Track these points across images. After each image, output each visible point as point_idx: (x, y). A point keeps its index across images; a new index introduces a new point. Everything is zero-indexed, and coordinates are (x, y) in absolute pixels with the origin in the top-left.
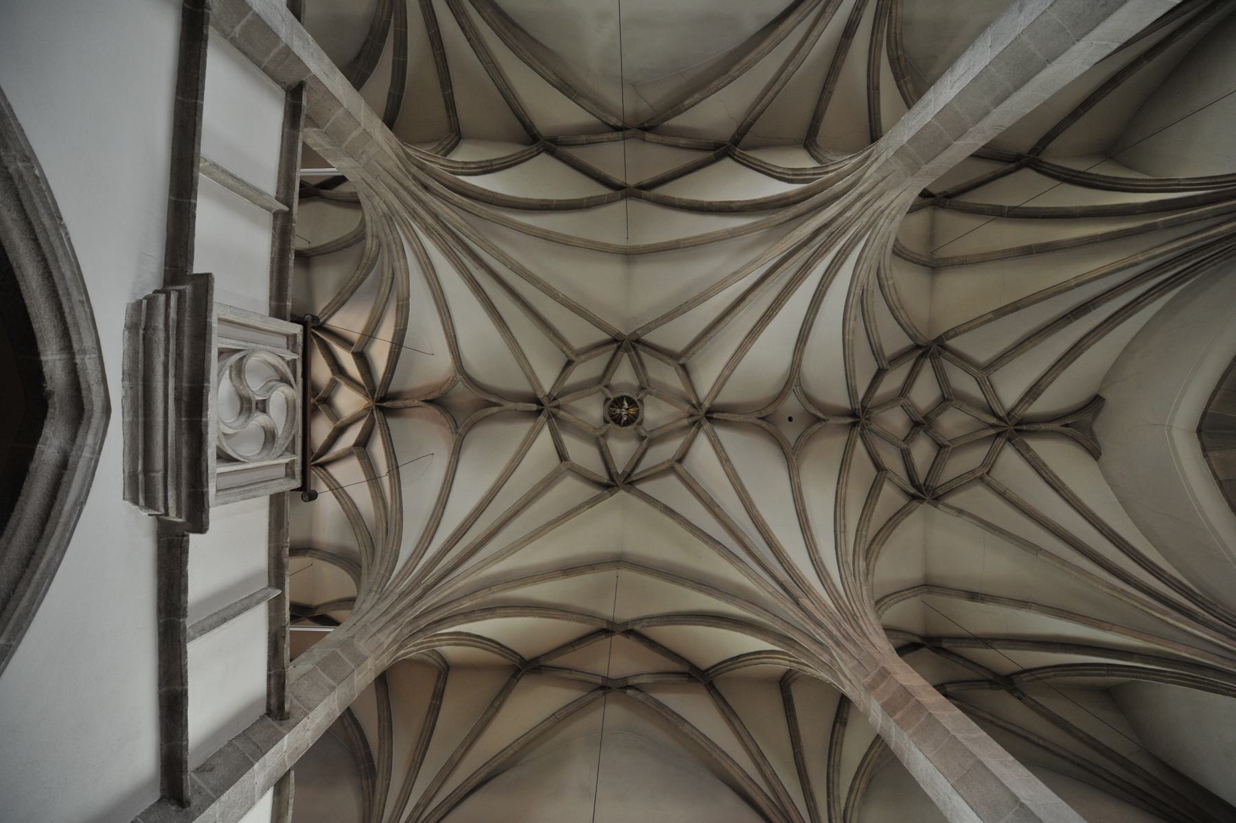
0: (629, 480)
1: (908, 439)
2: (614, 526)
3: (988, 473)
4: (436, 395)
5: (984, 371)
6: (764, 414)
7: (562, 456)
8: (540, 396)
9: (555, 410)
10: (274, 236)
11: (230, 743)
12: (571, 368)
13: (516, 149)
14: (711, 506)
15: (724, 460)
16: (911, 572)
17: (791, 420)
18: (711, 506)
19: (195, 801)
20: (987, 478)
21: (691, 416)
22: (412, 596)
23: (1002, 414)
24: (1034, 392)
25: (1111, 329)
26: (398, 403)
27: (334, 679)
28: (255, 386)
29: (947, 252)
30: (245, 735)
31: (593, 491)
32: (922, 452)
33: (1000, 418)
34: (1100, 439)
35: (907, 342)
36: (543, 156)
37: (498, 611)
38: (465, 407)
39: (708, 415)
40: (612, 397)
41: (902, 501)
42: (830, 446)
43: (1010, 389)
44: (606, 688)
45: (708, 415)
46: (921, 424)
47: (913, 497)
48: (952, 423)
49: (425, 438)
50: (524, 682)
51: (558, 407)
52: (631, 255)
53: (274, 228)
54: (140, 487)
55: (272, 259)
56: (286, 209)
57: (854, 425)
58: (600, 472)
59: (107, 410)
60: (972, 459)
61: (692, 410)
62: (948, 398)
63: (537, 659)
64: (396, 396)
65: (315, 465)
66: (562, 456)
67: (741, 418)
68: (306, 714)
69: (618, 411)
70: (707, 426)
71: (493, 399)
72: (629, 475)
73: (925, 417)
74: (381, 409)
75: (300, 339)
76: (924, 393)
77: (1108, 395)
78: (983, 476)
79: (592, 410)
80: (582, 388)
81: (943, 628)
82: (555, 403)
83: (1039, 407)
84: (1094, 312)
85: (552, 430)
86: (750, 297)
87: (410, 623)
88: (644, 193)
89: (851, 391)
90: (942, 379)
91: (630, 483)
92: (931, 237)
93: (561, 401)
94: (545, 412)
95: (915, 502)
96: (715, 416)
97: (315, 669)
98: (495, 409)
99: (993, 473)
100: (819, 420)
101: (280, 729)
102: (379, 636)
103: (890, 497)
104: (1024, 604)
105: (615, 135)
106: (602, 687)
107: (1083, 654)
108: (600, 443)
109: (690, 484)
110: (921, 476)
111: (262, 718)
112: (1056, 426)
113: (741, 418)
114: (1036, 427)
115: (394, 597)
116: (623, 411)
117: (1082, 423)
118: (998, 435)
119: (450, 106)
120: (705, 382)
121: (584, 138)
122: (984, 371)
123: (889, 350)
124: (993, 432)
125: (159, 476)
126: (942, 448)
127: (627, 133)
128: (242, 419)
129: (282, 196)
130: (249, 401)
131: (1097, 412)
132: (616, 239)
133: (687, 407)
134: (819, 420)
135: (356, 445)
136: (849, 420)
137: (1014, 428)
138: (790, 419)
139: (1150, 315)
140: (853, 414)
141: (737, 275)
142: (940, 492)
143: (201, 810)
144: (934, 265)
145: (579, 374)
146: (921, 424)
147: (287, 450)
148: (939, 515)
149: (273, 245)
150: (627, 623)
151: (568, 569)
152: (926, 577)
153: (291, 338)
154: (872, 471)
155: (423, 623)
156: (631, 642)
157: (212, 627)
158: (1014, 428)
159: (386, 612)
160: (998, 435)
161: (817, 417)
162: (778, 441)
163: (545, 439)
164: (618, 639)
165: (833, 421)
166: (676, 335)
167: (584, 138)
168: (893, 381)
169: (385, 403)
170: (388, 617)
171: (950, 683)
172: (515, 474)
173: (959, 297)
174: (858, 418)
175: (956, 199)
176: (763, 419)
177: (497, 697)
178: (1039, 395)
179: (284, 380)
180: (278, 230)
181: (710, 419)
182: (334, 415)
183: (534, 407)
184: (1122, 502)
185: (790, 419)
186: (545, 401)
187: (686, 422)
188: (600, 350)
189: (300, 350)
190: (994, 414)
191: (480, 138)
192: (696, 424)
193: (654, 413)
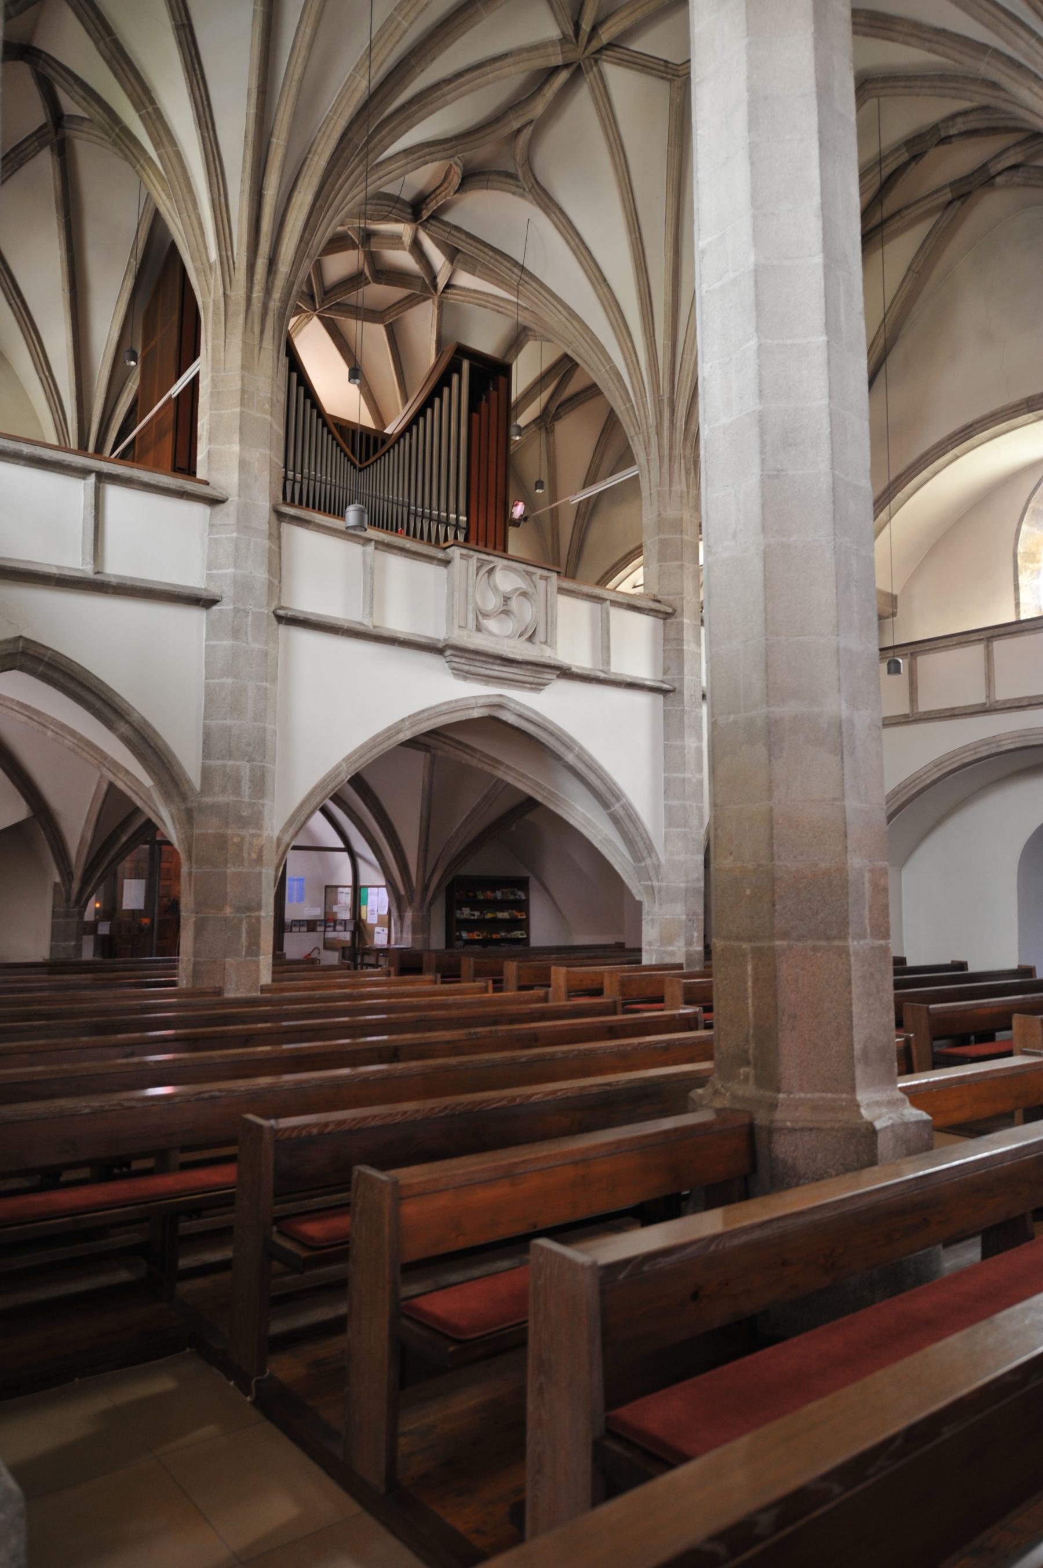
9: (595, 45)
11: (664, 651)
19: (677, 685)
22: (666, 424)
27: (677, 559)
28: (492, 602)
30: (666, 640)
54: (537, 686)
56: (373, 543)
59: (501, 696)
68: (682, 599)
82: (584, 37)
85: (621, 62)
87: (685, 439)
97: (661, 566)
101: (678, 620)
102: (674, 488)
111: (664, 624)
125: (536, 680)
143: (682, 685)
157: (609, 657)
159: (661, 458)
163: (619, 79)
164: (933, 153)
170: (666, 459)
172: (633, 176)
179: (491, 571)
183: (563, 76)
189: (471, 553)
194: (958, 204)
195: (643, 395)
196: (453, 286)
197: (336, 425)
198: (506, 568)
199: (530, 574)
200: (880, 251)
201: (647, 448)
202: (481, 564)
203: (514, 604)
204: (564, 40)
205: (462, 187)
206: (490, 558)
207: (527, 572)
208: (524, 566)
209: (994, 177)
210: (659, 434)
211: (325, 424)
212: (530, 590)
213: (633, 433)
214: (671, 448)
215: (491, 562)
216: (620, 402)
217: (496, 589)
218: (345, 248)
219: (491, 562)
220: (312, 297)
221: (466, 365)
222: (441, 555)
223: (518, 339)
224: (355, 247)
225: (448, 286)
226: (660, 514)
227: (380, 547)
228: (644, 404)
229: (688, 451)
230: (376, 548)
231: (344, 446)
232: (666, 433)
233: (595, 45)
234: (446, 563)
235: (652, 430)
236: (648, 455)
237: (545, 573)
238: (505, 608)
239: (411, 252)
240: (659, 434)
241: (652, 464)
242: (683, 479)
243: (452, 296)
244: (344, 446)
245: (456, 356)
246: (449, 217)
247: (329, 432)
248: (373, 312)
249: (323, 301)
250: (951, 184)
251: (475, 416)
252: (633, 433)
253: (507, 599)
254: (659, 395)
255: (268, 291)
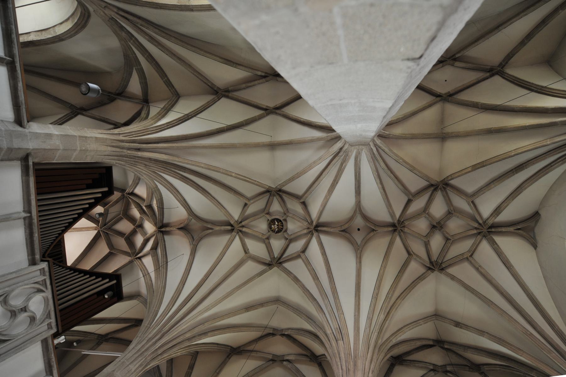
0: (279, 262)
1: (429, 235)
2: (273, 284)
3: (471, 256)
4: (182, 226)
5: (471, 198)
6: (343, 228)
7: (246, 251)
8: (232, 223)
9: (241, 229)
10: (25, 228)
12: (246, 208)
13: (210, 98)
14: (316, 277)
15: (324, 253)
16: (427, 308)
17: (357, 230)
18: (316, 277)
20: (470, 259)
21: (308, 228)
22: (154, 340)
23: (481, 222)
24: (497, 211)
25: (537, 180)
26: (167, 229)
28: (16, 302)
29: (449, 130)
31: (261, 267)
32: (437, 242)
33: (480, 224)
34: (537, 238)
35: (424, 183)
36: (223, 100)
37: (209, 334)
38: (197, 230)
39: (317, 228)
40: (270, 219)
41: (422, 270)
42: (380, 243)
43: (486, 208)
44: (276, 360)
45: (317, 228)
46: (437, 226)
47: (429, 269)
48: (454, 226)
49: (178, 245)
50: (234, 358)
51: (243, 226)
52: (273, 146)
53: (25, 225)
55: (26, 239)
56: (29, 215)
57: (395, 231)
58: (267, 258)
60: (463, 247)
61: (309, 226)
62: (451, 213)
63: (239, 347)
64: (167, 225)
65: (136, 258)
66: (246, 251)
67: (332, 230)
69: (273, 226)
70: (315, 234)
71: (209, 226)
72: (280, 259)
73: (439, 223)
74: (162, 232)
75: (47, 269)
76: (438, 209)
77: (541, 212)
78: (469, 257)
79: (262, 226)
80: (254, 215)
81: (444, 337)
82: (241, 225)
83: (503, 217)
84: (526, 170)
86: (324, 174)
88: (278, 111)
89: (392, 214)
90: (449, 202)
91: (280, 263)
92: (442, 120)
93: (243, 223)
94: (235, 230)
95: (429, 271)
96: (319, 229)
98: (211, 231)
99: (474, 256)
100: (373, 230)
103: (415, 269)
104: (481, 332)
105: (264, 80)
106: (272, 360)
107: (520, 360)
108: (266, 241)
109: (308, 263)
110: (434, 258)
112: (511, 229)
113: (332, 230)
114: (500, 230)
115: (145, 341)
116: (277, 226)
117: (527, 228)
118: (479, 233)
119: (169, 84)
120: (314, 211)
121: (244, 86)
122: (471, 198)
123: (413, 188)
124: (475, 232)
126: (448, 240)
127: (267, 79)
128: (12, 320)
129: (26, 209)
130: (14, 311)
131: (537, 221)
132: (265, 139)
133: (306, 224)
134: (373, 230)
135: (152, 249)
136: (391, 229)
137: (488, 230)
138: (359, 230)
139: (562, 171)
140: (393, 225)
141: (315, 163)
142: (444, 266)
144: (442, 137)
145: (251, 210)
146: (437, 226)
147: (47, 318)
148: (442, 277)
149: (25, 232)
150: (282, 330)
151: (248, 308)
152: (436, 310)
153: (42, 271)
154: (406, 255)
155: (160, 352)
156: (284, 339)
158: (488, 230)
159: (139, 350)
160: (479, 233)
161: (373, 227)
162: (352, 242)
163: (237, 242)
164: (278, 338)
165: (380, 230)
166: (299, 186)
167: (244, 86)
168: (418, 205)
169: (163, 228)
170: (139, 353)
171: (449, 365)
172: (221, 263)
173: (457, 156)
174: (397, 227)
175: (455, 96)
176: (344, 230)
177: (219, 367)
178: (500, 213)
180: (27, 225)
181: (317, 231)
182: (144, 233)
183: (229, 228)
184: (545, 277)
185: (359, 230)
186: (235, 225)
187: (305, 231)
188: (261, 197)
189: (47, 274)
190: (477, 222)
191: (189, 95)
192: (311, 233)
193: (292, 226)
194: (271, 362)
195: (157, 326)
196: (141, 260)
197: (60, 241)
198: (46, 300)
199: (49, 316)
200: (245, 360)
201: (139, 343)
202: (44, 283)
203: (23, 316)
204: (237, 222)
205: (180, 229)
206: (49, 286)
207: (49, 314)
208: (53, 309)
209: (284, 361)
210: (148, 341)
211: (60, 234)
212: (37, 322)
213: (139, 335)
214: (146, 350)
215: (47, 288)
216: (147, 322)
217: (28, 299)
218: (131, 222)
219: (47, 288)
220: (105, 225)
221: (115, 282)
222: (38, 257)
223: (135, 296)
224: (134, 225)
225: (140, 258)
226: (114, 371)
227: (27, 221)
228: (154, 328)
229: (149, 358)
230: (25, 218)
231: (50, 249)
232: (150, 343)
233: (241, 229)
234: (33, 262)
235: (147, 339)
236: (136, 346)
237: (54, 324)
238: (17, 311)
239: (144, 240)
240: (148, 341)
241: (133, 350)
242: (137, 366)
243: (137, 262)
244: (50, 249)
245: (116, 277)
246: (166, 238)
247: (57, 237)
248: (112, 246)
249: (106, 229)
250: (273, 355)
251: (96, 296)
252: (139, 335)
253: (24, 309)
254: (162, 329)
255: (129, 149)
